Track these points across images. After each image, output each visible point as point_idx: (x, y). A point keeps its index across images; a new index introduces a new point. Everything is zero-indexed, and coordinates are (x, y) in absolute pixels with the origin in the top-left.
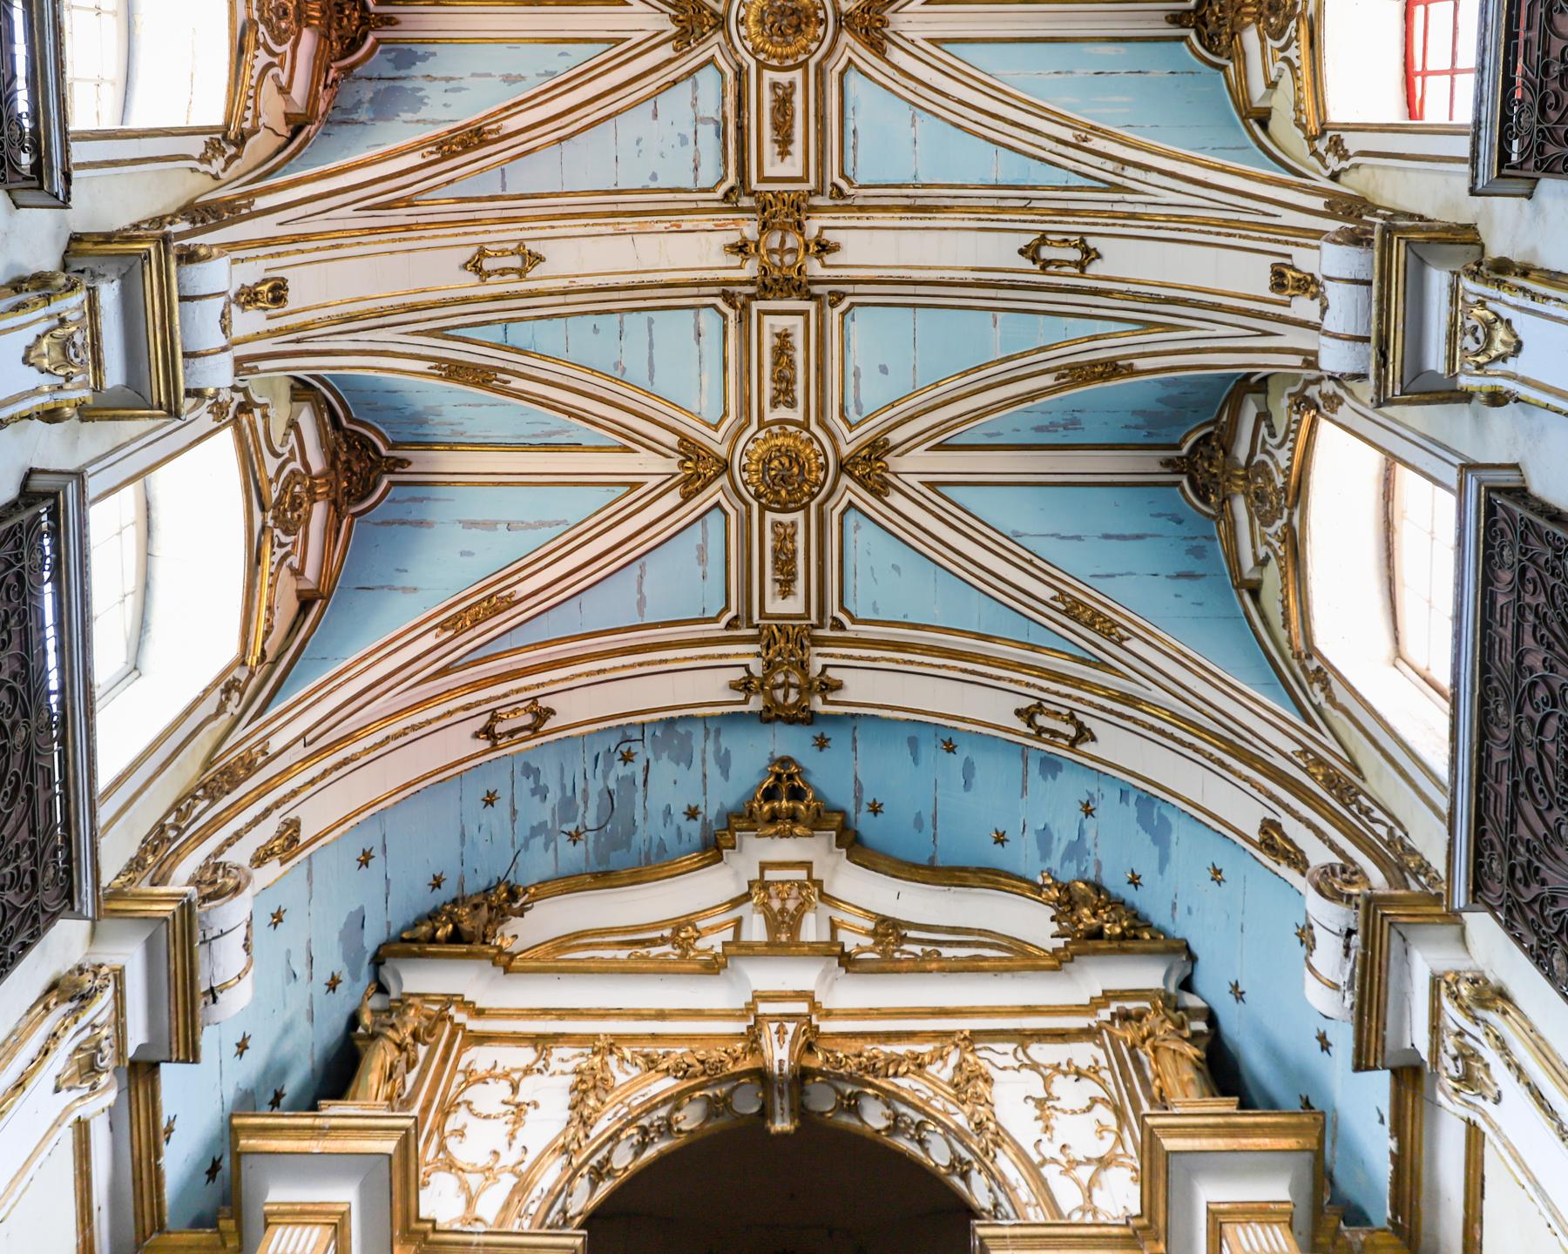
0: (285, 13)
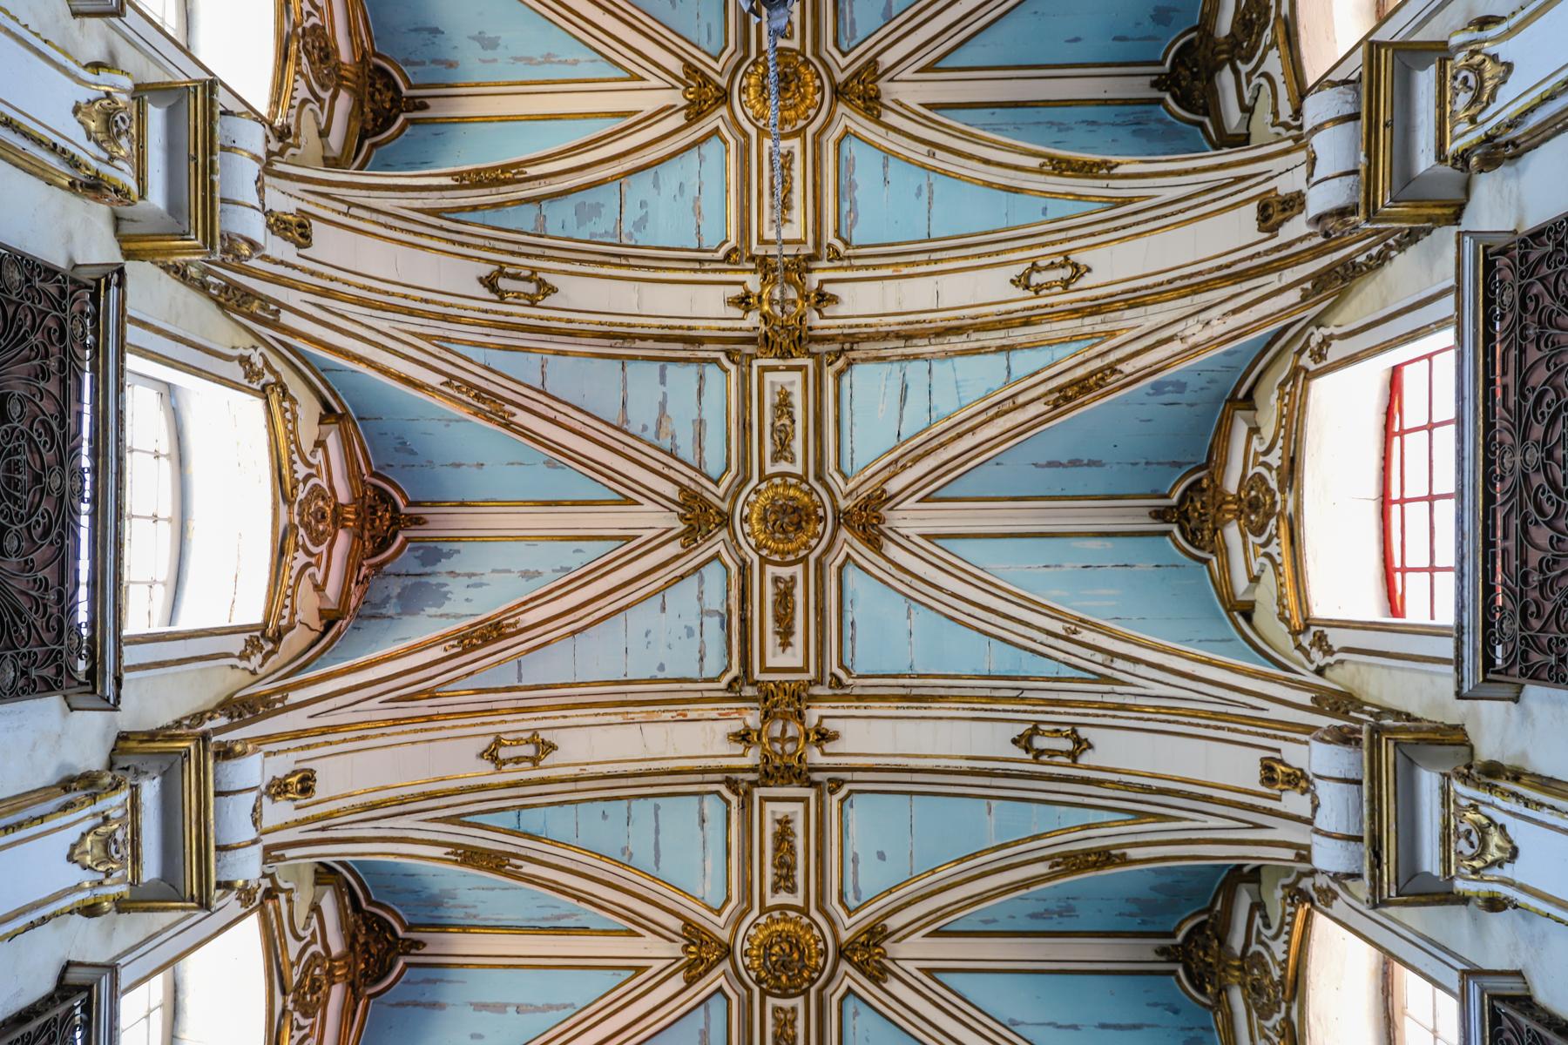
0: (323, 517)
